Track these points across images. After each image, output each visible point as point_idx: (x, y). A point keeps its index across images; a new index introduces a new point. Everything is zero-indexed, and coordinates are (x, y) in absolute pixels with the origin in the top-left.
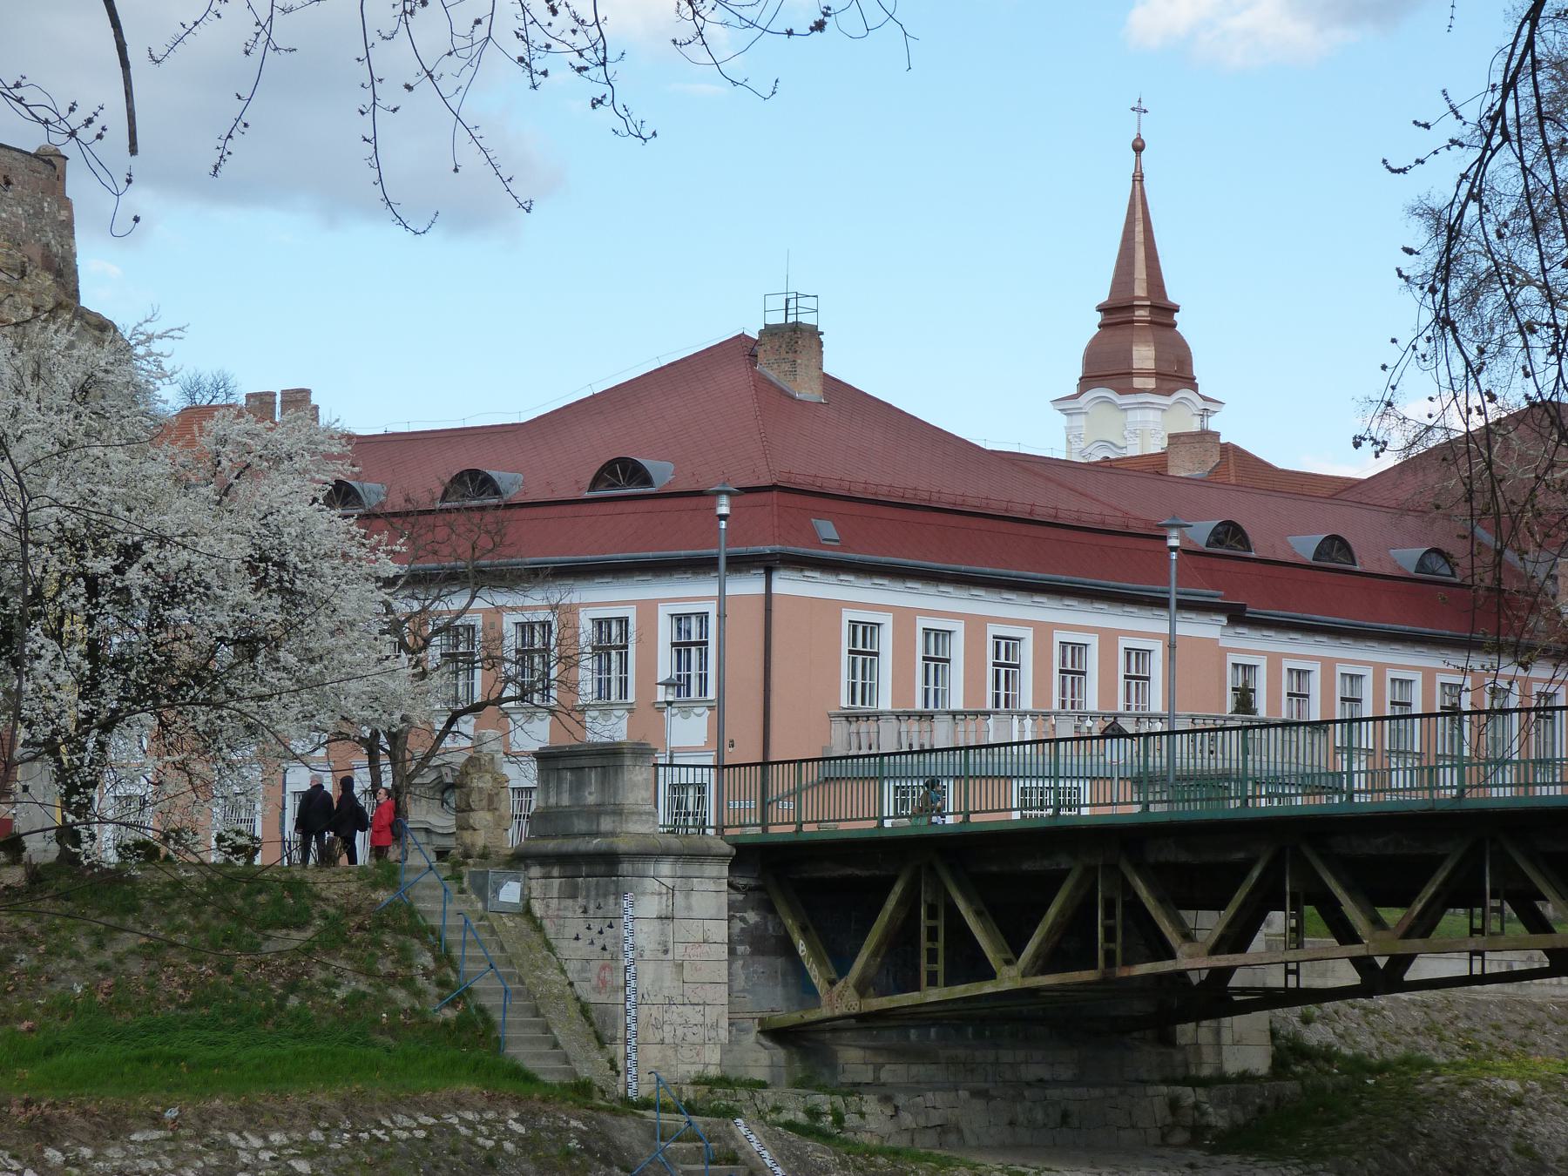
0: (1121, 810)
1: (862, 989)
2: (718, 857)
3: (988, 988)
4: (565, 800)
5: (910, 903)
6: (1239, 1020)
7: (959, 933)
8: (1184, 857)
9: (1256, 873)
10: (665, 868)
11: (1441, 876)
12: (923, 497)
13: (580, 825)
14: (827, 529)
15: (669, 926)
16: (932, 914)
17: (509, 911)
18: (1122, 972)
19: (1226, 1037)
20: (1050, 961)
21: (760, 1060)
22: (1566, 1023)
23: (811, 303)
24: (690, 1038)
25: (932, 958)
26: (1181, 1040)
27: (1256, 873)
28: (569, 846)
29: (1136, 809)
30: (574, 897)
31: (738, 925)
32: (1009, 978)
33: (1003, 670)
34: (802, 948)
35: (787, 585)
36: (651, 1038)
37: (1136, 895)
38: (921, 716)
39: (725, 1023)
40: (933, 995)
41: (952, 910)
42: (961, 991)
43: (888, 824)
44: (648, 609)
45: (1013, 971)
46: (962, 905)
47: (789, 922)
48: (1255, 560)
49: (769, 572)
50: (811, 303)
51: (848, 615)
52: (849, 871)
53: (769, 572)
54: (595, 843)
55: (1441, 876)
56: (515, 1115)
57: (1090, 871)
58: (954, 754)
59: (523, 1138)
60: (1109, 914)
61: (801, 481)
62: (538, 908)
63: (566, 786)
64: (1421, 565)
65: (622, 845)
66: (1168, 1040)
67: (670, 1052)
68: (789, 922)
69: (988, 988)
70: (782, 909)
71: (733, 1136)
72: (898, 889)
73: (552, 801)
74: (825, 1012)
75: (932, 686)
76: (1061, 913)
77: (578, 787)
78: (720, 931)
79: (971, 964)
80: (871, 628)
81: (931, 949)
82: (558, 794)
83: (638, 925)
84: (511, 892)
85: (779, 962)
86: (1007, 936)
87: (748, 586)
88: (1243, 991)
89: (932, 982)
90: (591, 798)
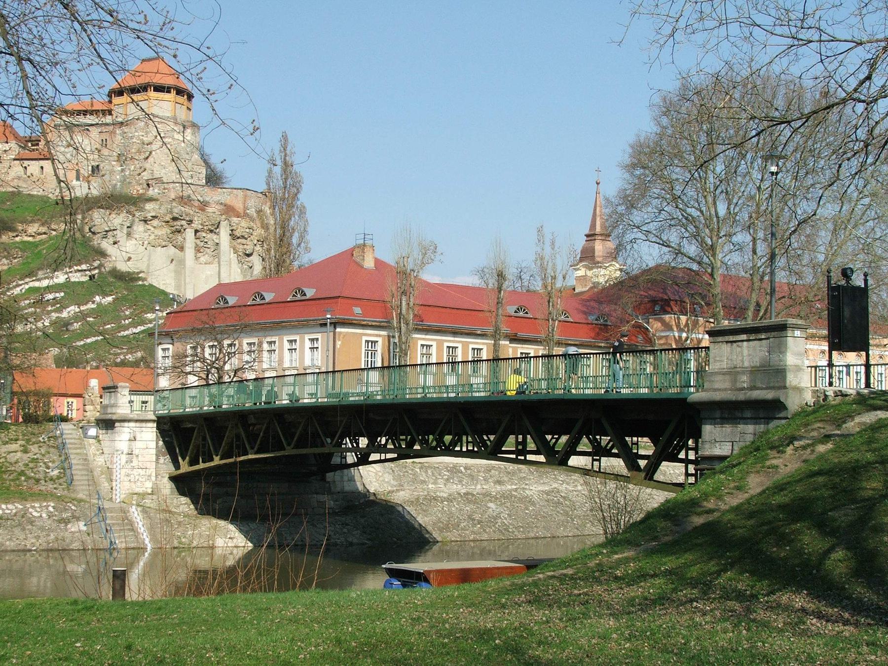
0: (178, 411)
2: (154, 421)
14: (358, 310)
15: (133, 443)
22: (2, 551)
23: (370, 237)
24: (140, 479)
26: (328, 480)
29: (181, 411)
33: (370, 352)
36: (126, 479)
39: (154, 474)
43: (205, 408)
48: (268, 304)
50: (370, 237)
56: (53, 505)
58: (326, 380)
65: (114, 417)
66: (323, 479)
71: (129, 511)
75: (370, 359)
90: (112, 402)
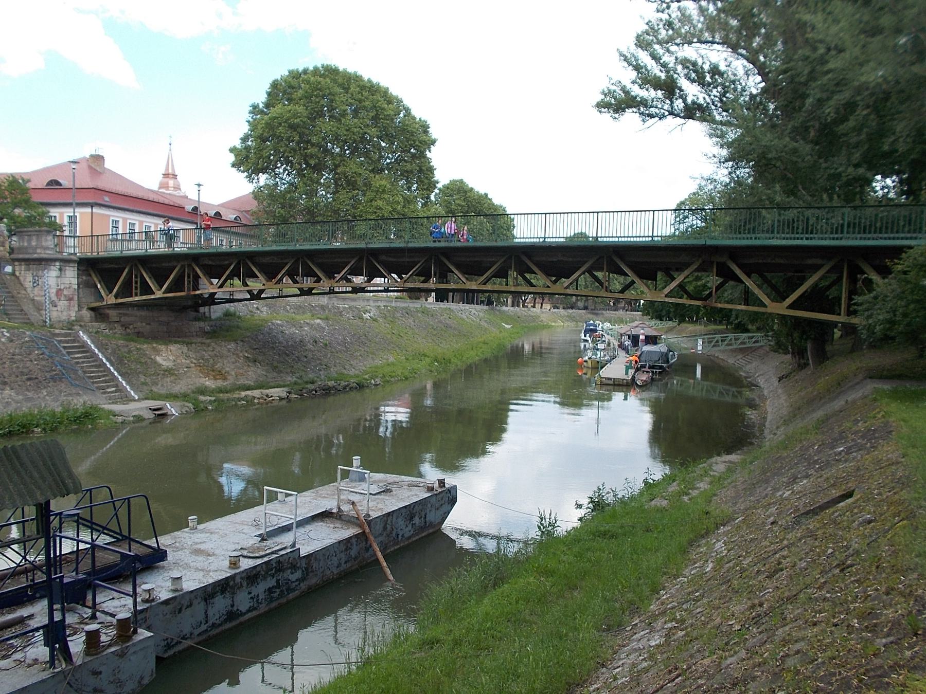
1: (116, 297)
3: (153, 297)
4: (26, 244)
5: (130, 273)
6: (215, 307)
7: (144, 283)
8: (210, 263)
9: (232, 267)
10: (57, 264)
11: (286, 268)
12: (129, 194)
13: (31, 251)
14: (107, 199)
15: (59, 279)
16: (136, 277)
17: (9, 274)
18: (193, 293)
19: (212, 310)
20: (168, 290)
21: (86, 314)
25: (136, 288)
27: (232, 267)
28: (27, 256)
30: (29, 270)
31: (80, 280)
32: (159, 294)
34: (99, 286)
35: (95, 210)
37: (196, 272)
38: (128, 241)
40: (137, 299)
41: (142, 276)
42: (144, 297)
44: (62, 215)
45: (161, 292)
46: (145, 275)
47: (95, 279)
49: (92, 207)
51: (112, 218)
52: (112, 266)
53: (92, 207)
54: (35, 256)
55: (286, 268)
57: (183, 267)
59: (8, 337)
60: (189, 277)
61: (100, 188)
62: (17, 273)
63: (26, 240)
64: (235, 219)
67: (60, 313)
68: (95, 279)
69: (153, 297)
70: (93, 275)
72: (126, 270)
73: (21, 244)
74: (105, 303)
76: (174, 277)
77: (29, 241)
78: (75, 281)
79: (147, 290)
80: (117, 222)
81: (136, 285)
82: (23, 242)
83: (49, 279)
84: (9, 269)
85: (93, 290)
86: (158, 283)
87: (89, 210)
88: (218, 299)
89: (136, 295)
